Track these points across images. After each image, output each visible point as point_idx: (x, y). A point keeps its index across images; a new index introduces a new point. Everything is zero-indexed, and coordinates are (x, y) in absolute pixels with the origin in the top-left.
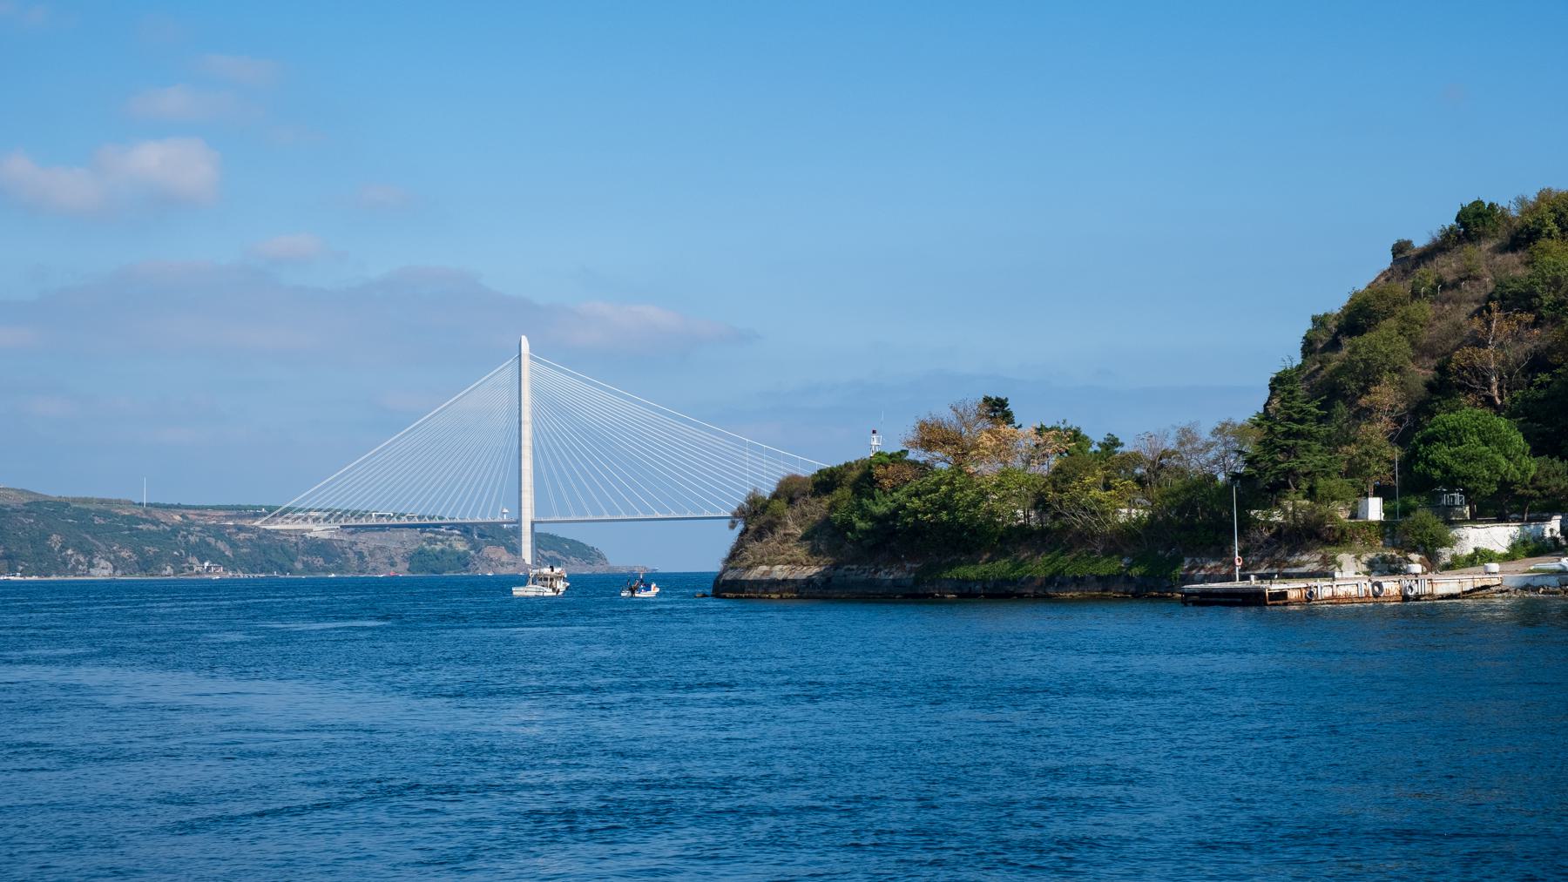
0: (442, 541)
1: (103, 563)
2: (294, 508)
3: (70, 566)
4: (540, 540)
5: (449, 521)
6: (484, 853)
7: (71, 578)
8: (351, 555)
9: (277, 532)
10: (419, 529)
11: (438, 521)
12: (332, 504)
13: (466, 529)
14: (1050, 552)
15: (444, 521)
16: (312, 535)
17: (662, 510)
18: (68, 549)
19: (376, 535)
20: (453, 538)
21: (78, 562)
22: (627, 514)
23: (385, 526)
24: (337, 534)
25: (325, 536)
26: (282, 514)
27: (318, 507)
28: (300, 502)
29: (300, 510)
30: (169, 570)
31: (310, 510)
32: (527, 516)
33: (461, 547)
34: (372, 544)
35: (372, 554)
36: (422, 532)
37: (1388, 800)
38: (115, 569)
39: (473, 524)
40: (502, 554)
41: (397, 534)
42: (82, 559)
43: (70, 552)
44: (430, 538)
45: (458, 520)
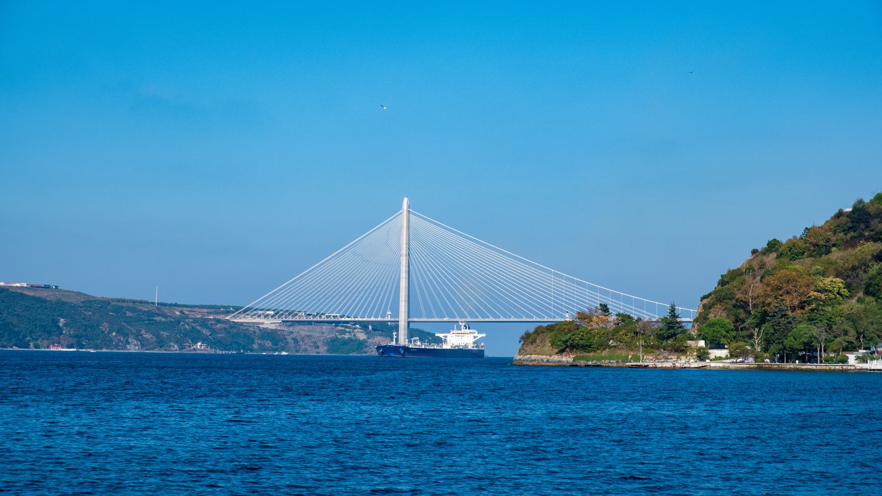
0: (349, 332)
8: (290, 340)
9: (241, 324)
10: (334, 324)
16: (264, 326)
19: (306, 328)
20: (356, 331)
21: (119, 340)
24: (280, 326)
25: (273, 327)
26: (245, 311)
27: (262, 308)
28: (257, 304)
33: (362, 336)
34: (303, 333)
35: (303, 340)
36: (336, 326)
39: (369, 322)
41: (318, 328)
43: (114, 334)
44: (341, 330)
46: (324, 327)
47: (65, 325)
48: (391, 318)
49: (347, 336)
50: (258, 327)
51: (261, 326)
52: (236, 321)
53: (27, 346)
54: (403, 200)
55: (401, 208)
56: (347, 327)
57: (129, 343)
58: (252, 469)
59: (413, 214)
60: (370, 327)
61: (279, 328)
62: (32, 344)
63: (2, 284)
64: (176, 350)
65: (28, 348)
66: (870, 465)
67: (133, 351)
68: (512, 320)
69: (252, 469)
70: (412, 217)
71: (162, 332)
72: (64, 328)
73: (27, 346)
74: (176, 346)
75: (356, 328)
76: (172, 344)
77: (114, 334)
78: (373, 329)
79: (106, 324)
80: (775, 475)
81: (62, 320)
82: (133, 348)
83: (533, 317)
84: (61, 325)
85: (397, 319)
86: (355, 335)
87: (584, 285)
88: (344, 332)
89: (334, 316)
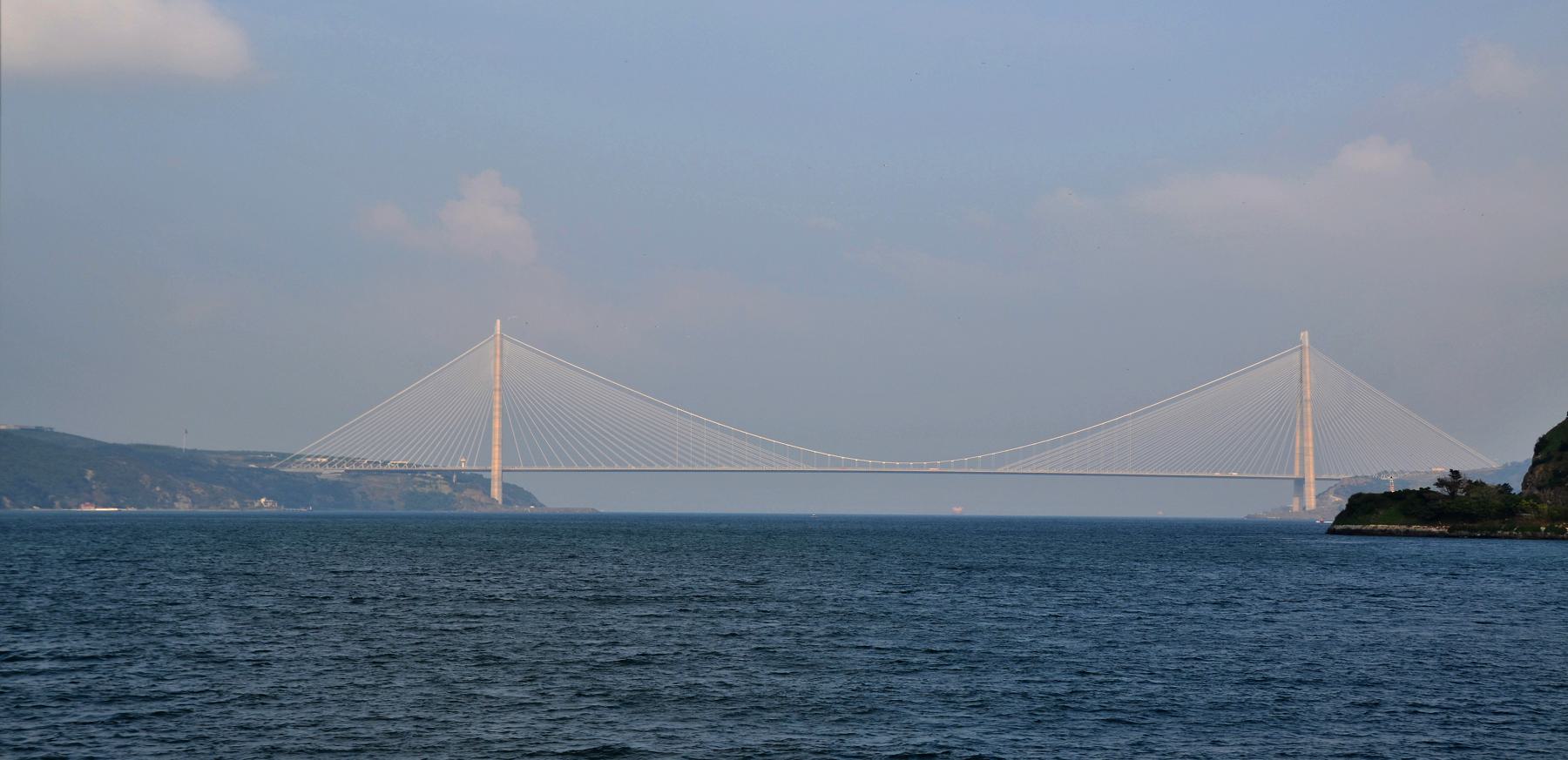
1: (185, 498)
2: (289, 455)
3: (159, 500)
4: (506, 488)
5: (433, 468)
6: (1139, 709)
7: (161, 510)
9: (294, 474)
11: (425, 468)
12: (315, 451)
13: (448, 475)
14: (481, 476)
15: (429, 468)
16: (322, 477)
17: (634, 463)
18: (155, 486)
21: (165, 497)
22: (620, 465)
23: (382, 471)
25: (333, 478)
26: (292, 459)
27: (325, 454)
28: (309, 450)
29: (309, 457)
30: (236, 504)
31: (317, 457)
32: (496, 466)
33: (446, 489)
37: (837, 718)
38: (193, 503)
39: (453, 471)
40: (477, 496)
42: (168, 495)
43: (158, 489)
45: (440, 467)
46: (398, 479)
47: (93, 478)
48: (477, 465)
49: (427, 490)
50: (316, 478)
51: (318, 476)
52: (287, 470)
53: (51, 505)
54: (496, 322)
55: (493, 330)
56: (426, 478)
57: (177, 500)
58: (73, 670)
59: (507, 339)
60: (455, 477)
61: (341, 479)
62: (57, 503)
63: (3, 427)
64: (236, 508)
65: (51, 508)
66: (139, 712)
67: (182, 510)
68: (668, 468)
69: (73, 670)
70: (506, 343)
71: (215, 486)
72: (94, 482)
73: (51, 505)
74: (236, 503)
75: (437, 479)
76: (231, 501)
77: (158, 489)
78: (458, 480)
79: (146, 477)
80: (533, 716)
81: (90, 472)
82: (183, 506)
83: (627, 465)
84: (88, 478)
85: (489, 468)
86: (437, 488)
87: (702, 422)
88: (424, 484)
89: (400, 465)
